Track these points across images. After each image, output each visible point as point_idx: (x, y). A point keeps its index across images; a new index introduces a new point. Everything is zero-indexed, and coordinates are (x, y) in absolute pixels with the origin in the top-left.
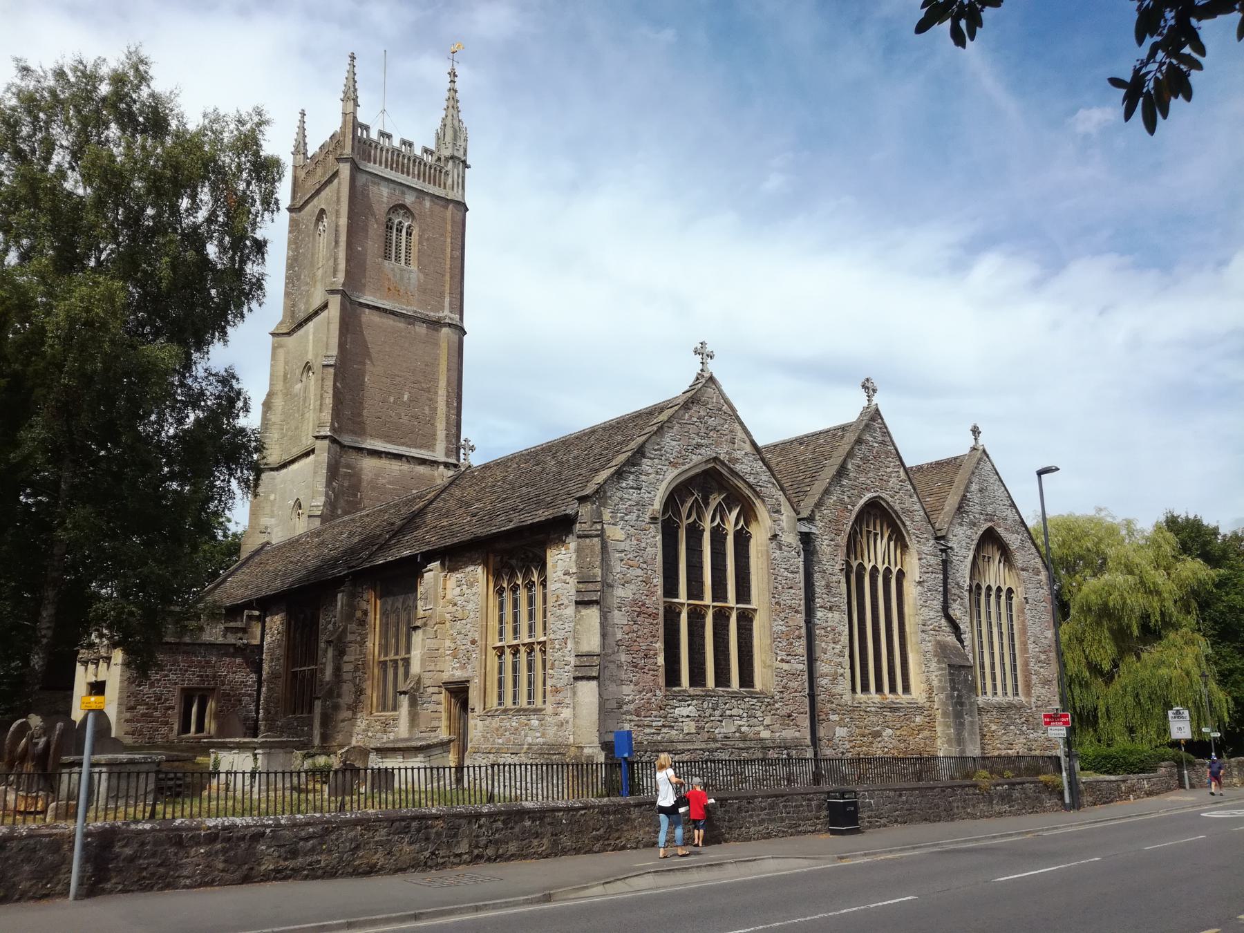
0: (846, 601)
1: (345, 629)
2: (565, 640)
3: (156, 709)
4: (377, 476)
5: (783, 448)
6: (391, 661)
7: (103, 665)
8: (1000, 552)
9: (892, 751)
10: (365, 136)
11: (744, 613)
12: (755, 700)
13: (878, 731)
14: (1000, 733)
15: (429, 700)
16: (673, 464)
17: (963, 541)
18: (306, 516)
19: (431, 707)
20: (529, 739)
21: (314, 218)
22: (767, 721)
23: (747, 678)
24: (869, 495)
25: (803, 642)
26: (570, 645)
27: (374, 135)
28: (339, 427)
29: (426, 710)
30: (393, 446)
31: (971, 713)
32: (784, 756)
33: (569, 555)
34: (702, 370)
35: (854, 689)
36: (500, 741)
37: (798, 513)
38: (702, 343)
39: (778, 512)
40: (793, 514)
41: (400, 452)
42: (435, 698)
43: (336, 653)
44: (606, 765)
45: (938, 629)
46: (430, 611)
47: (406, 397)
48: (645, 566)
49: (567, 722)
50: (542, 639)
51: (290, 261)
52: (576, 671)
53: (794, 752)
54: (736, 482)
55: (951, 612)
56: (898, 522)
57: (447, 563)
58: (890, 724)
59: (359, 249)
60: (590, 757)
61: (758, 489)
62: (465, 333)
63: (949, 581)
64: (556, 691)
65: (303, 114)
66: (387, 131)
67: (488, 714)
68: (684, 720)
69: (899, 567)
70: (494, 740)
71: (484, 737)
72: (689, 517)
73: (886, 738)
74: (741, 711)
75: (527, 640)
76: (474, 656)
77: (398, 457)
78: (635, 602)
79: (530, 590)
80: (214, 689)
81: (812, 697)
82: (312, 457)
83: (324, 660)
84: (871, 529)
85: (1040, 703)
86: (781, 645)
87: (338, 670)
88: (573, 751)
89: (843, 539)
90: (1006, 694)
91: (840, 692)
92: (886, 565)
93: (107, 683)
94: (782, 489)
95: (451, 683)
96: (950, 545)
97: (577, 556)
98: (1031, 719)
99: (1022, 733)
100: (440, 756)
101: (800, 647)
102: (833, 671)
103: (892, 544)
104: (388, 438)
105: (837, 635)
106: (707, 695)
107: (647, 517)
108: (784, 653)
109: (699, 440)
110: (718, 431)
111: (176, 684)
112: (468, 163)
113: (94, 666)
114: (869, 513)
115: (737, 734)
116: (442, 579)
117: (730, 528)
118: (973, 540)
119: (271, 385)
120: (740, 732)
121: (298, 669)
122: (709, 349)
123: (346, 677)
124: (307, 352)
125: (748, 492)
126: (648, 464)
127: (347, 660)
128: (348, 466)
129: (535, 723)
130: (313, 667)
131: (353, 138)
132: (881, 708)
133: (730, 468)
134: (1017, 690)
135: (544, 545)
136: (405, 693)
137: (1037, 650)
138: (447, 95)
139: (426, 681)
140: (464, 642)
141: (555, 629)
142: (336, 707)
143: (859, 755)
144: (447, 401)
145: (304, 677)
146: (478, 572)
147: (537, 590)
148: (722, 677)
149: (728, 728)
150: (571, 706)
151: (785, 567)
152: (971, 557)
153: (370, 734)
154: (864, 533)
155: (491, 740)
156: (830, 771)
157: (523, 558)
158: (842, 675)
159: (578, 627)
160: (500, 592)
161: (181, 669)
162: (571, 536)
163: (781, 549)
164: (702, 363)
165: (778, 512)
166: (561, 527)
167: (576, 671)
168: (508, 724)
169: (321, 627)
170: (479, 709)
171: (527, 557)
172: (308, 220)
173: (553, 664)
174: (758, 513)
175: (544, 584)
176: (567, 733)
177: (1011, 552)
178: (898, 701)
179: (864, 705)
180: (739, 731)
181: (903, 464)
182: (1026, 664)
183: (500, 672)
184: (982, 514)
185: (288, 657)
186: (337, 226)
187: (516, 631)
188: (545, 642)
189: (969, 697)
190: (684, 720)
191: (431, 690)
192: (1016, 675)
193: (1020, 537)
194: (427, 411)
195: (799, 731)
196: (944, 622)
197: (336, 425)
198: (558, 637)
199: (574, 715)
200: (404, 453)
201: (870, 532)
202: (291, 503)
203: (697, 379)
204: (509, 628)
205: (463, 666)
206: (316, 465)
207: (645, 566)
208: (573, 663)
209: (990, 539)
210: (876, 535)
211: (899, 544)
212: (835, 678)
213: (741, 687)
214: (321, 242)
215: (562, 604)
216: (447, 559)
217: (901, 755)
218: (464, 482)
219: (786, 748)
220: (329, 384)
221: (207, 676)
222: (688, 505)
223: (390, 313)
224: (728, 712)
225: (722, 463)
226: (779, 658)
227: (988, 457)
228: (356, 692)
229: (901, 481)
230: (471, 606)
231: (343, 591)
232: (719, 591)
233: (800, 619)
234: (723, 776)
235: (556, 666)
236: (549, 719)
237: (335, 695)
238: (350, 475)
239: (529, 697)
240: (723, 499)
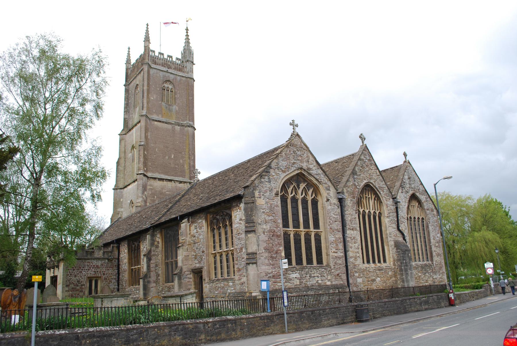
0: (359, 226)
1: (151, 249)
2: (241, 249)
3: (78, 286)
4: (162, 189)
5: (328, 164)
6: (170, 262)
7: (56, 269)
8: (418, 203)
9: (380, 287)
10: (153, 55)
11: (317, 233)
12: (324, 269)
13: (374, 279)
14: (422, 277)
15: (186, 277)
16: (284, 172)
17: (403, 198)
18: (135, 206)
19: (187, 280)
20: (229, 291)
21: (134, 88)
22: (329, 277)
23: (320, 261)
24: (365, 181)
25: (342, 244)
26: (244, 250)
27: (157, 54)
28: (146, 170)
29: (185, 281)
30: (168, 177)
31: (410, 269)
32: (337, 292)
33: (241, 212)
34: (293, 132)
35: (363, 262)
36: (217, 292)
37: (337, 190)
38: (292, 121)
39: (329, 190)
40: (335, 191)
41: (171, 179)
42: (188, 276)
43: (148, 260)
44: (262, 299)
45: (396, 236)
46: (184, 240)
47: (173, 157)
48: (274, 215)
49: (244, 283)
50: (232, 249)
51: (125, 106)
52: (247, 261)
53: (341, 290)
54: (311, 178)
55: (400, 228)
56: (378, 192)
57: (190, 219)
58: (379, 276)
59: (152, 98)
60: (256, 296)
61: (320, 180)
62: (195, 129)
63: (399, 216)
64: (239, 270)
65: (129, 48)
66: (161, 52)
67: (211, 281)
68: (294, 279)
69: (379, 211)
70: (214, 292)
71: (210, 291)
72: (291, 193)
73: (378, 282)
74: (318, 274)
75: (225, 250)
76: (204, 258)
77: (170, 180)
78: (270, 231)
79: (225, 228)
80: (100, 277)
81: (347, 266)
82: (136, 183)
83: (143, 263)
84: (367, 196)
85: (437, 263)
86: (333, 246)
87: (148, 266)
88: (248, 294)
89: (355, 200)
90: (424, 261)
91: (359, 264)
92: (374, 210)
93: (58, 276)
94: (330, 181)
95: (195, 269)
96: (399, 201)
97: (245, 212)
98: (434, 270)
99: (431, 276)
100: (191, 299)
101: (341, 246)
102: (355, 255)
103: (376, 201)
104: (166, 173)
105: (356, 240)
106: (303, 269)
107: (274, 194)
108: (335, 249)
109: (294, 161)
110: (302, 157)
111: (85, 275)
112: (194, 63)
113: (53, 270)
114: (365, 189)
115: (317, 284)
116: (188, 226)
117: (309, 198)
118: (407, 199)
119: (120, 155)
120: (318, 283)
121: (133, 267)
122: (296, 123)
123: (152, 269)
124: (133, 141)
125: (316, 182)
126: (273, 171)
127: (152, 262)
128: (151, 185)
129: (231, 284)
130: (139, 266)
131: (149, 56)
132: (375, 269)
133: (307, 172)
134: (428, 259)
135: (230, 208)
136: (176, 274)
137: (435, 242)
138: (185, 37)
139: (184, 269)
140: (199, 252)
141: (237, 244)
142: (149, 282)
143: (367, 289)
144: (189, 157)
145: (136, 271)
146: (203, 223)
147: (228, 228)
148: (310, 261)
149: (313, 282)
150: (246, 276)
151: (333, 213)
152: (407, 206)
153: (163, 292)
154: (364, 198)
155: (213, 292)
156: (356, 297)
157: (222, 215)
158: (359, 257)
159: (247, 242)
160: (213, 230)
161: (87, 269)
162: (242, 204)
163: (331, 206)
164: (293, 129)
165: (329, 190)
166: (238, 198)
167: (247, 261)
168: (220, 285)
169: (141, 250)
170: (207, 280)
171: (224, 214)
172: (132, 89)
173: (237, 259)
174: (320, 191)
175: (231, 225)
176: (245, 287)
177: (423, 203)
178: (382, 266)
179: (368, 269)
180: (317, 282)
181: (378, 169)
182: (431, 248)
183: (215, 263)
184: (410, 188)
185: (129, 263)
186: (143, 90)
187: (220, 246)
188: (233, 250)
189: (410, 263)
190: (294, 279)
191: (187, 273)
192: (427, 253)
193: (425, 196)
194: (181, 161)
195: (343, 281)
196: (398, 232)
197: (145, 169)
198: (239, 247)
199: (247, 279)
200: (173, 179)
201: (366, 197)
202: (129, 202)
203: (292, 135)
204: (217, 245)
205: (200, 262)
206: (138, 185)
207: (274, 215)
208: (245, 258)
209: (414, 197)
210: (369, 198)
211: (378, 201)
212: (356, 258)
213: (317, 264)
214: (137, 97)
215: (240, 233)
216: (190, 218)
217: (384, 288)
218: (197, 187)
219: (337, 288)
220: (142, 152)
221: (97, 272)
222: (291, 188)
223: (165, 123)
224: (313, 275)
225: (305, 170)
226: (333, 251)
227: (411, 165)
228: (157, 276)
229: (378, 175)
230: (201, 237)
231: (149, 234)
232: (306, 225)
233: (340, 235)
234: (312, 301)
235: (239, 260)
236: (237, 282)
237: (148, 277)
238: (152, 189)
239: (228, 274)
240: (306, 186)
